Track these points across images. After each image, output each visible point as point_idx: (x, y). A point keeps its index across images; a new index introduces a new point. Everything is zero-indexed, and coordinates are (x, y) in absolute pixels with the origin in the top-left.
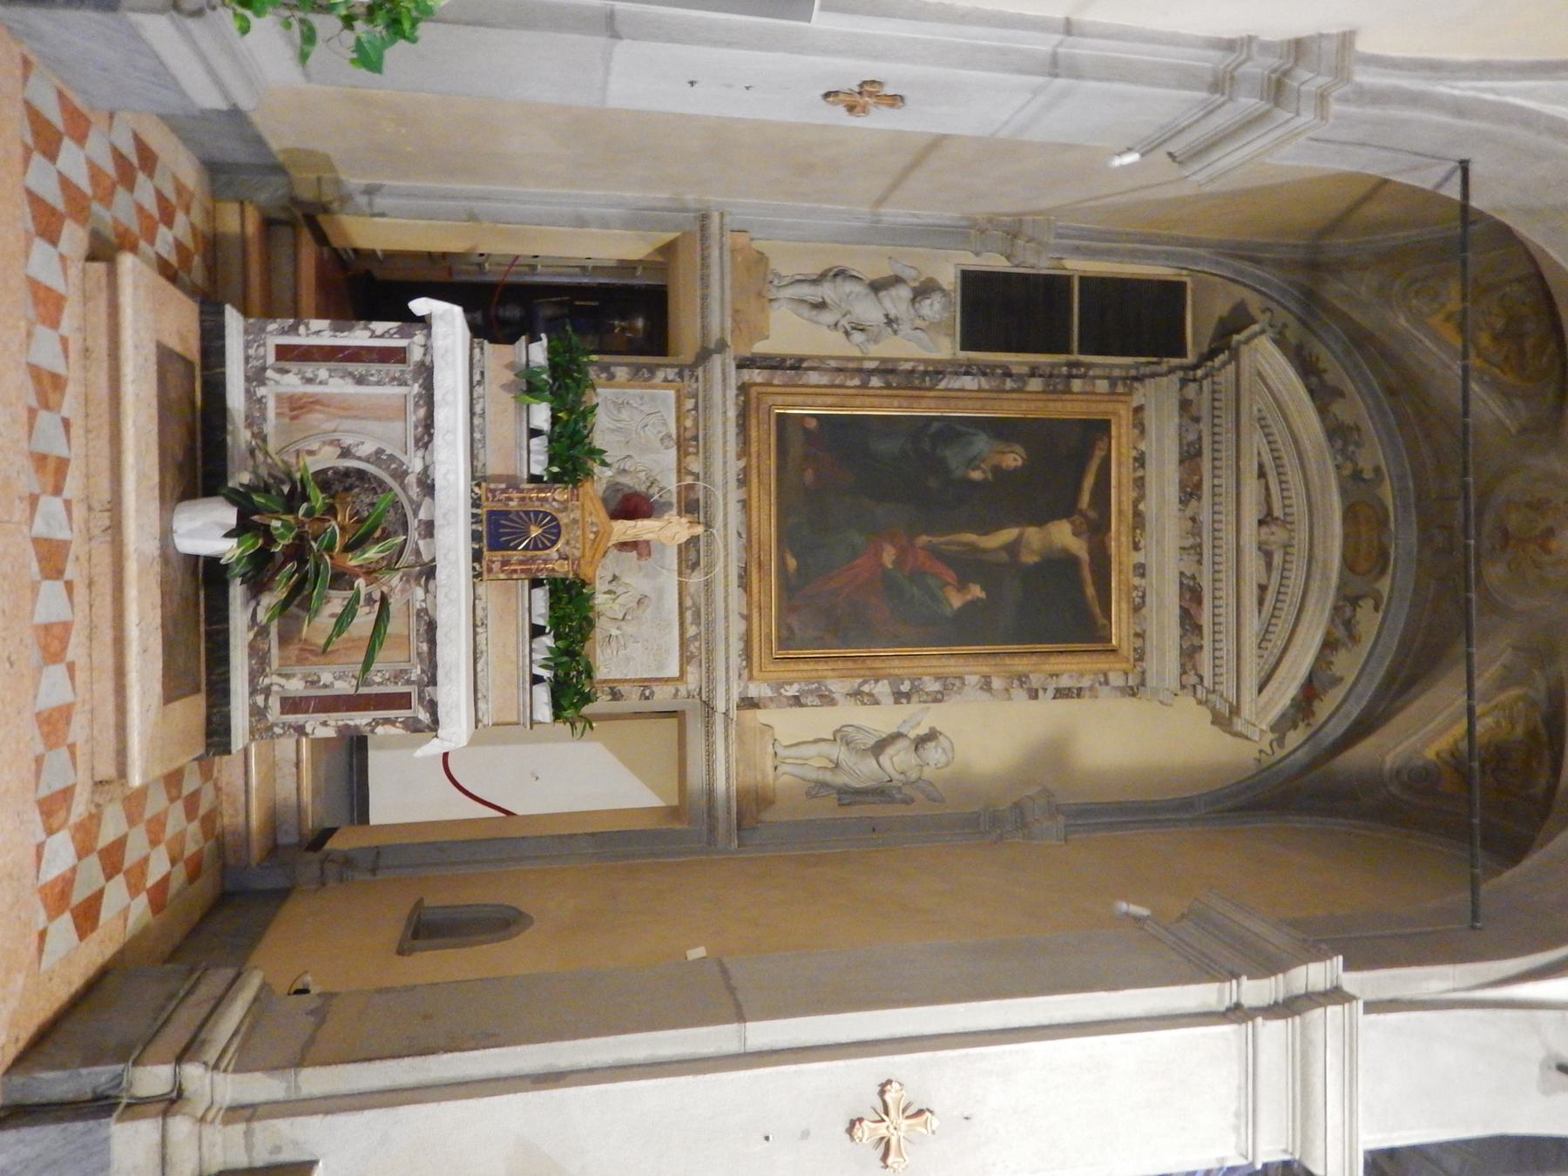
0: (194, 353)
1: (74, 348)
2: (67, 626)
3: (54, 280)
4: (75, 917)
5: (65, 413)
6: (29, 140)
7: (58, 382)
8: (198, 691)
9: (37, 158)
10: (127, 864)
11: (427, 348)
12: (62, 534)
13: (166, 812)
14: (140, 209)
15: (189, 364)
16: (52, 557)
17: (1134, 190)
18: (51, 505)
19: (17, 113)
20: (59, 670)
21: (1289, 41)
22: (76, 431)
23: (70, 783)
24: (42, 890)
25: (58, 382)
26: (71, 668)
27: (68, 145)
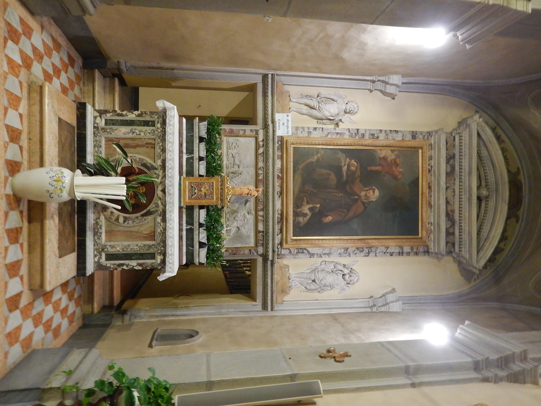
0: (74, 123)
1: (25, 85)
2: (21, 228)
3: (17, 91)
4: (22, 312)
5: (21, 111)
6: (7, 35)
7: (18, 99)
8: (74, 251)
9: (10, 43)
10: (44, 320)
11: (104, 373)
12: (18, 159)
13: (60, 299)
14: (53, 65)
15: (74, 127)
16: (14, 135)
17: (287, 182)
18: (11, 112)
19: (2, 25)
20: (17, 279)
21: (250, 286)
22: (25, 119)
23: (20, 258)
24: (6, 300)
25: (18, 99)
26: (22, 245)
27: (23, 38)
